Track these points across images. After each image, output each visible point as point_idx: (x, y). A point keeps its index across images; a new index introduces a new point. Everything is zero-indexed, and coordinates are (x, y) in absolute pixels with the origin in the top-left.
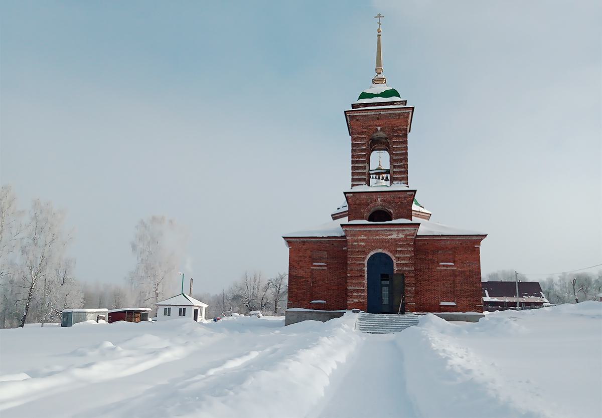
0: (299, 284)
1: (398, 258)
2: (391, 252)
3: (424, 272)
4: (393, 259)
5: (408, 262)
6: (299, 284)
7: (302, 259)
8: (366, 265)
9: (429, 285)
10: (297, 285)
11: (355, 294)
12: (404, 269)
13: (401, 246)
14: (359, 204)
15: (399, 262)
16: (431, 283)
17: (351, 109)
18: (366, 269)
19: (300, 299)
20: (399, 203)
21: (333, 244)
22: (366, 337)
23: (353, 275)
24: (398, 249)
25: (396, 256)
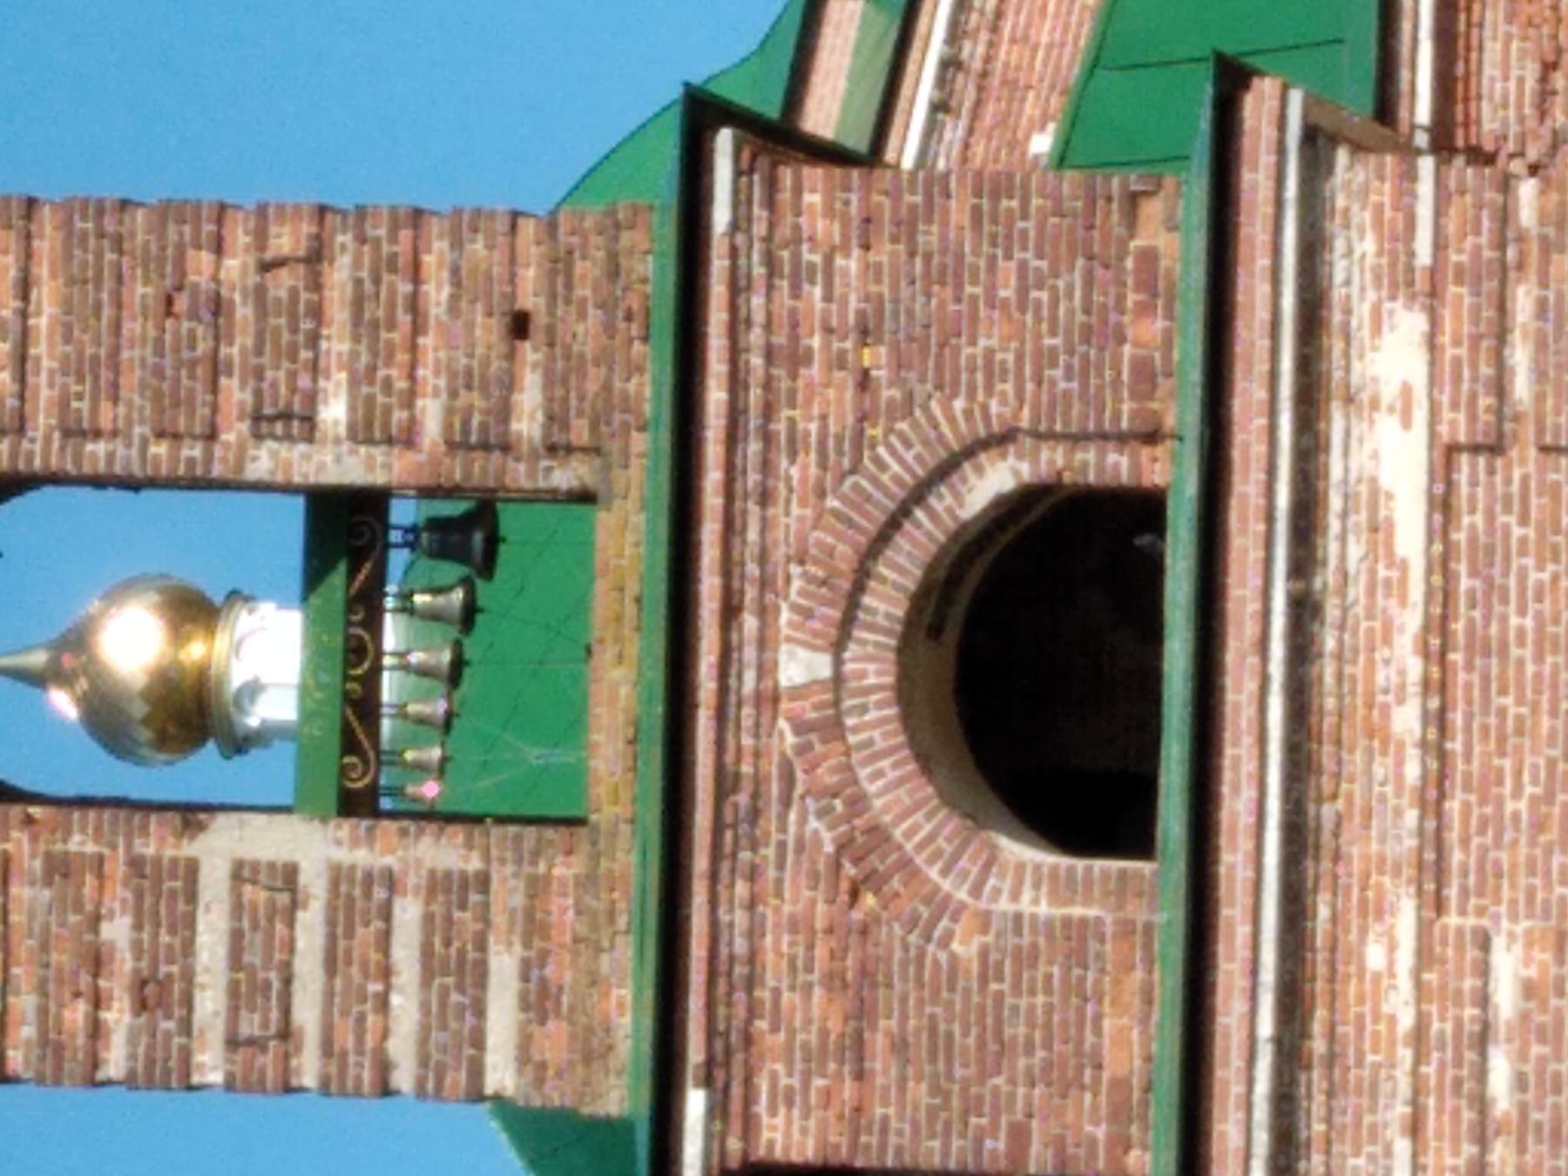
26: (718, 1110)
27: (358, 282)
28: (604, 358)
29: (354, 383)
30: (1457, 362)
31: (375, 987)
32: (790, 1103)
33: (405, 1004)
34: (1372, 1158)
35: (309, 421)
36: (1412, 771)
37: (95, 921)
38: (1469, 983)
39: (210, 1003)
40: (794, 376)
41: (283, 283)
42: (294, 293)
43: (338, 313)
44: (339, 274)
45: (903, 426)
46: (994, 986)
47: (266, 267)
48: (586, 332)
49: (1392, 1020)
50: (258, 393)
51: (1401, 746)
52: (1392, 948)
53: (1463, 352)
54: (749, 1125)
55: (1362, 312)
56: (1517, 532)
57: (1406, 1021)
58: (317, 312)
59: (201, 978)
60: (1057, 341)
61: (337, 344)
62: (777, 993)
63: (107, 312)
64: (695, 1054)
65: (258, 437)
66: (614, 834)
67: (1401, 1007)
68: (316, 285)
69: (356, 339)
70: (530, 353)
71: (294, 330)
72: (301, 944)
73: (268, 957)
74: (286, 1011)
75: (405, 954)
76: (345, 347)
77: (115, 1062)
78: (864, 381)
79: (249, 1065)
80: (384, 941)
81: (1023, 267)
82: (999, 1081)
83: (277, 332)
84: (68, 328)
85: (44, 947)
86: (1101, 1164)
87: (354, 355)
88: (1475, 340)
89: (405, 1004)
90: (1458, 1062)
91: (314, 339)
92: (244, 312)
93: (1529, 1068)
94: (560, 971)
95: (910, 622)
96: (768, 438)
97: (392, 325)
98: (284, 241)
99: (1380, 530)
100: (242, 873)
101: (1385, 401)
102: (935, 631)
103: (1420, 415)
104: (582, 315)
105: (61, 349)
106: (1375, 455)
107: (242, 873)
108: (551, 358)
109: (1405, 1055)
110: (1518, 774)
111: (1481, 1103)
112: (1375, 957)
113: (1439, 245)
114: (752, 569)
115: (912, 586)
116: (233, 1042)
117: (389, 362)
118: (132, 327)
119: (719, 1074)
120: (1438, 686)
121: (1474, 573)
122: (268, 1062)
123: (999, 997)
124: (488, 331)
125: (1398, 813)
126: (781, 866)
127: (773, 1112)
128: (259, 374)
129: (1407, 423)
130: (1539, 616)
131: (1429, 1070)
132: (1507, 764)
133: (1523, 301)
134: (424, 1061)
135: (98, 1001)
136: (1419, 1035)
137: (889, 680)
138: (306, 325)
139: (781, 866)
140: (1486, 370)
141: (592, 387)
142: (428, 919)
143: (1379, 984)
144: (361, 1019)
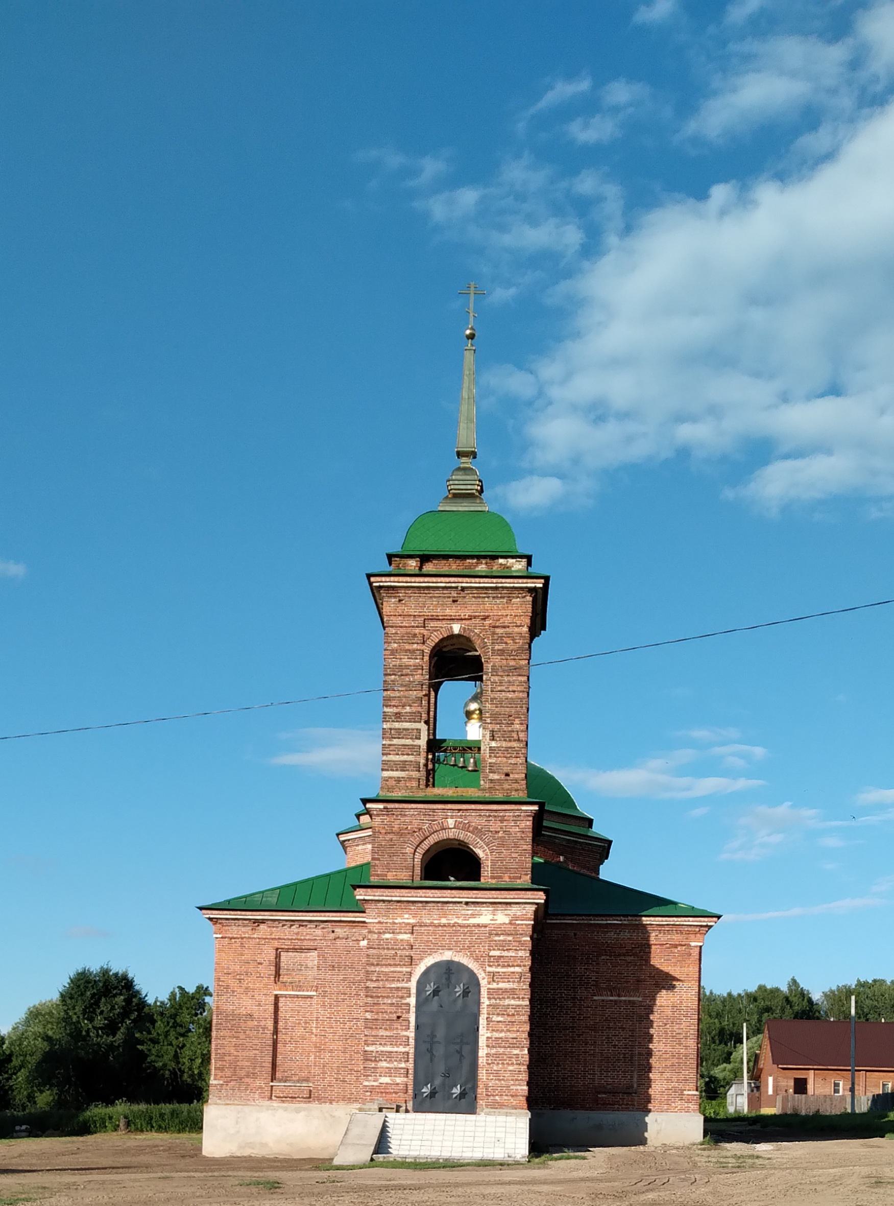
0: (242, 1036)
1: (493, 977)
2: (477, 959)
3: (561, 1007)
4: (480, 977)
5: (515, 986)
6: (242, 1036)
7: (251, 968)
8: (414, 991)
9: (574, 1041)
10: (237, 1038)
11: (384, 1064)
12: (507, 1002)
13: (502, 946)
14: (400, 834)
15: (494, 986)
16: (579, 1036)
17: (386, 568)
18: (412, 1001)
19: (243, 1073)
20: (500, 834)
21: (333, 932)
22: (212, 1098)
23: (380, 1016)
24: (492, 953)
25: (489, 969)
26: (381, 810)
27: (514, 748)
28: (503, 789)
29: (498, 747)
30: (501, 928)
31: (400, 753)
32: (382, 822)
33: (397, 758)
34: (375, 916)
35: (493, 740)
36: (436, 922)
37: (410, 706)
38: (402, 931)
39: (397, 725)
40: (499, 820)
41: (515, 735)
42: (513, 737)
43: (509, 744)
44: (515, 744)
45: (491, 838)
46: (401, 855)
47: (518, 732)
48: (506, 786)
49: (396, 919)
50: (496, 731)
51: (440, 920)
52: (408, 919)
53: (503, 929)
54: (378, 815)
55: (509, 912)
56: (474, 938)
57: (396, 921)
58: (510, 741)
59: (401, 723)
60: (504, 864)
61: (504, 744)
62: (400, 819)
63: (510, 706)
64: (390, 806)
65: (490, 731)
66: (425, 792)
67: (399, 920)
68: (515, 740)
69: (506, 748)
70: (503, 777)
71: (508, 737)
72: (407, 740)
73: (405, 735)
74: (395, 738)
75: (405, 758)
76: (504, 746)
77: (386, 709)
78: (497, 832)
79: (387, 732)
80: (408, 755)
81: (517, 858)
82: (386, 856)
83: (506, 734)
84: (507, 699)
85: (405, 697)
86: (543, 832)
87: (503, 747)
88: (505, 931)
89: (397, 758)
90: (390, 929)
91: (505, 740)
92: (510, 729)
93: (389, 941)
94: (402, 784)
95: (459, 840)
96: (490, 816)
97: (508, 754)
98: (522, 735)
99: (473, 916)
100: (419, 730)
101: (495, 917)
102: (459, 844)
103: (493, 922)
104: (509, 785)
105: (504, 698)
106: (486, 915)
107: (419, 730)
108: (503, 780)
109: (391, 921)
110: (436, 938)
111: (384, 933)
112: (406, 916)
113: (519, 925)
114: (468, 814)
115: (465, 841)
116: (391, 729)
117: (502, 753)
118: (508, 709)
119: (386, 810)
120: (449, 925)
121: (468, 931)
122: (388, 735)
123: (399, 856)
124: (506, 769)
125: (429, 919)
126: (420, 820)
127: (381, 819)
128: (500, 731)
129: (491, 920)
130: (461, 941)
131: (389, 925)
132: (437, 937)
133: (510, 938)
134: (388, 761)
135: (396, 707)
136: (395, 923)
137: (450, 837)
138: (508, 739)
139: (420, 820)
140: (500, 932)
141: (497, 787)
142: (411, 761)
143: (402, 917)
144: (395, 751)
